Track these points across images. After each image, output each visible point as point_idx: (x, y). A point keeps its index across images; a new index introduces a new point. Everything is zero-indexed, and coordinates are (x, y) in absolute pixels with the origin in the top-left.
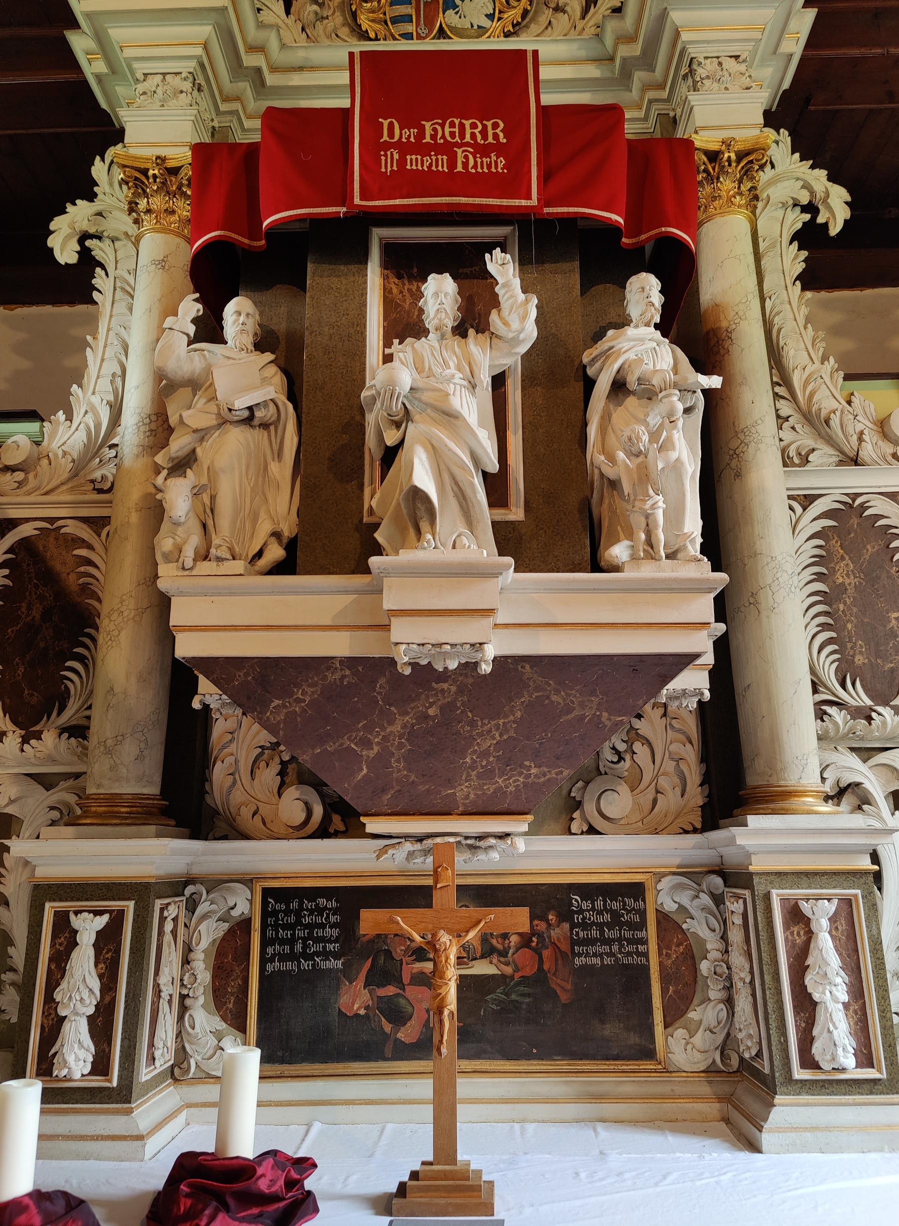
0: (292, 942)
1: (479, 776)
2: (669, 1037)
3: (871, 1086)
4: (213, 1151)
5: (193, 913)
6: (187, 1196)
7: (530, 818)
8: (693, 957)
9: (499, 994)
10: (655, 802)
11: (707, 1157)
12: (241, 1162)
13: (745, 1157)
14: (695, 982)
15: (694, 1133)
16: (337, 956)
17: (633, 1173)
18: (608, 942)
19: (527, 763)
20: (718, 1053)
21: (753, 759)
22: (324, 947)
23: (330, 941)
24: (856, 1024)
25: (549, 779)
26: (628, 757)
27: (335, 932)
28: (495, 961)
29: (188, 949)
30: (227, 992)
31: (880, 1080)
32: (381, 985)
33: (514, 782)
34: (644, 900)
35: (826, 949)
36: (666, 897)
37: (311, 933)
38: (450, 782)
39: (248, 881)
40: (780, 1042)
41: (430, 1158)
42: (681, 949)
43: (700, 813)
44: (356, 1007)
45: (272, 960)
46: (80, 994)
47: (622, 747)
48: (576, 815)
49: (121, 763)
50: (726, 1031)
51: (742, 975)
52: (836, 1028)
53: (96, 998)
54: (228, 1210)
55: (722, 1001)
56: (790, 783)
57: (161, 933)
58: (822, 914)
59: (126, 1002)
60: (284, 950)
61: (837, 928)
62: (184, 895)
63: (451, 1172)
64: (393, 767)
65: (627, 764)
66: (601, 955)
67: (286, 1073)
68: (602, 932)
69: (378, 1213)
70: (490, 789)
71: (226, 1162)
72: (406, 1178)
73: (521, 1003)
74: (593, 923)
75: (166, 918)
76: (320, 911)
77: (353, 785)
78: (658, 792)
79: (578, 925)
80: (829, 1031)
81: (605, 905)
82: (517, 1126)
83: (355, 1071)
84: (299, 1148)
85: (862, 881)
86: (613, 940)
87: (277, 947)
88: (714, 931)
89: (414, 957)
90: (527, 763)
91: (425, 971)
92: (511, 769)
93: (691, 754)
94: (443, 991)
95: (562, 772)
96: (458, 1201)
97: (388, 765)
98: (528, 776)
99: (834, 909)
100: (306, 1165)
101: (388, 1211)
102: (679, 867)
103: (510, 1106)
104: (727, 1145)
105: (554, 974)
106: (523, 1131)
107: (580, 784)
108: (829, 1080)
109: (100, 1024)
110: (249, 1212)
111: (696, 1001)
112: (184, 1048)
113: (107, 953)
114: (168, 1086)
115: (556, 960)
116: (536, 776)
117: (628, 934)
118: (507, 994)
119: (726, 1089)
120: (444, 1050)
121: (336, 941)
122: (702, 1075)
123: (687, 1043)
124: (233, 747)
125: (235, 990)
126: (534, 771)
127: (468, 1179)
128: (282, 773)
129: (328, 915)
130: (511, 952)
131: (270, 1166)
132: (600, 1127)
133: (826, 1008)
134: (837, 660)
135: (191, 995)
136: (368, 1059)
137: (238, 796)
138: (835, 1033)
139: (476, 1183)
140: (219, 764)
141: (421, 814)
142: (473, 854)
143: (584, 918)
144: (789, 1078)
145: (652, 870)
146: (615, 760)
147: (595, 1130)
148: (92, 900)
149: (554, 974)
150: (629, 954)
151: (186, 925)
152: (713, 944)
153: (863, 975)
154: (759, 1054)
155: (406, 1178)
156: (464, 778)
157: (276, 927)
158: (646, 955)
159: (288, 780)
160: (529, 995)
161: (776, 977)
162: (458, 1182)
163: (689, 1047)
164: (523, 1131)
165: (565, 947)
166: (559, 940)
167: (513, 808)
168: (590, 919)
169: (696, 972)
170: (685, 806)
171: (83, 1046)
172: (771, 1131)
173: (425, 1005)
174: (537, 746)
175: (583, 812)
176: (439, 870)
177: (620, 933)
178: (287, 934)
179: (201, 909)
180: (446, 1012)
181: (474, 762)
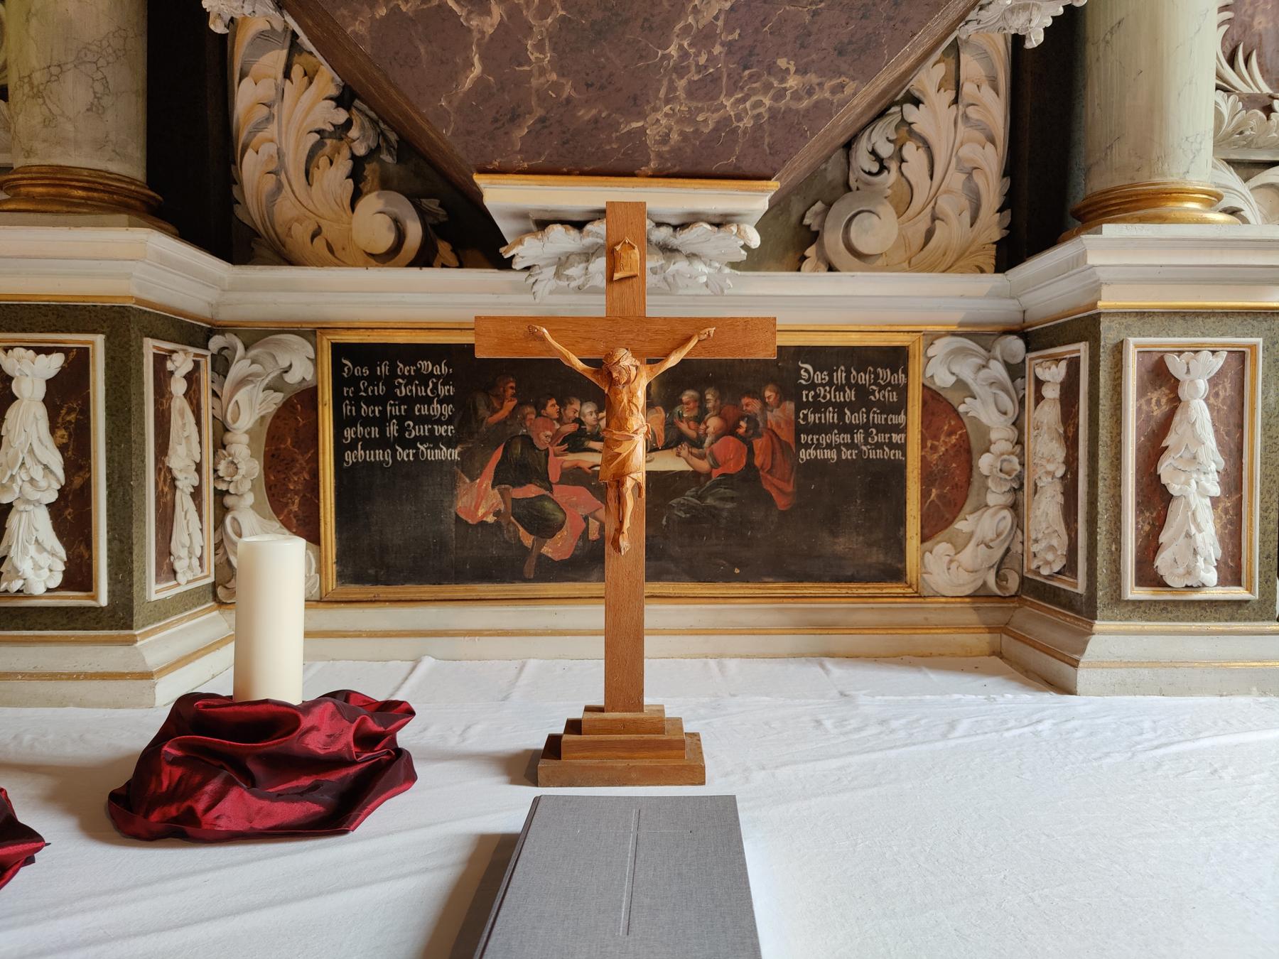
0: (382, 422)
1: (691, 93)
2: (927, 554)
3: (1234, 609)
4: (231, 694)
5: (225, 377)
6: (175, 762)
7: (774, 185)
8: (969, 451)
9: (689, 497)
10: (929, 234)
11: (1000, 699)
12: (273, 708)
13: (1050, 700)
14: (969, 483)
15: (962, 669)
16: (450, 443)
17: (903, 721)
18: (849, 429)
19: (782, 63)
20: (993, 572)
21: (1111, 147)
22: (431, 431)
23: (439, 422)
24: (1224, 527)
25: (817, 103)
26: (894, 166)
27: (447, 410)
28: (684, 452)
29: (222, 430)
30: (288, 490)
31: (1247, 601)
32: (518, 483)
33: (755, 106)
34: (906, 372)
35: (1199, 416)
36: (939, 368)
37: (410, 411)
38: (636, 105)
39: (310, 332)
40: (1110, 551)
41: (599, 701)
42: (954, 439)
43: (994, 253)
44: (481, 512)
45: (352, 447)
46: (28, 470)
47: (886, 150)
48: (810, 252)
49: (63, 114)
50: (1006, 545)
51: (1050, 467)
52: (1200, 531)
53: (58, 480)
54: (251, 781)
55: (1004, 507)
56: (1170, 179)
57: (162, 391)
58: (1199, 375)
59: (109, 486)
60: (370, 433)
61: (1217, 395)
62: (206, 348)
63: (634, 721)
64: (529, 62)
65: (891, 177)
66: (838, 447)
67: (383, 597)
68: (842, 416)
69: (514, 781)
70: (708, 120)
71: (245, 709)
72: (559, 729)
73: (723, 509)
74: (829, 403)
75: (172, 373)
76: (424, 379)
77: (456, 104)
78: (934, 218)
79: (807, 405)
80: (1188, 535)
81: (848, 378)
82: (712, 662)
83: (482, 595)
84: (398, 688)
85: (1265, 325)
86: (858, 427)
87: (360, 429)
88: (1005, 413)
89: (566, 446)
90: (782, 63)
91: (582, 465)
92: (751, 76)
93: (991, 160)
94: (623, 449)
95: (842, 87)
96: (647, 763)
97: (521, 59)
98: (780, 95)
99: (1221, 363)
100: (398, 712)
101: (532, 778)
102: (960, 325)
103: (702, 638)
104: (1014, 684)
105: (770, 472)
106: (722, 669)
107: (819, 206)
108: (1174, 601)
109: (70, 516)
110: (294, 783)
111: (967, 508)
112: (229, 562)
113: (68, 413)
114: (210, 610)
115: (773, 453)
116: (796, 96)
117: (879, 419)
118: (700, 498)
119: (998, 617)
120: (624, 543)
121: (449, 422)
122: (967, 600)
123: (951, 561)
124: (272, 130)
125: (300, 487)
126: (792, 82)
127: (661, 731)
128: (356, 174)
129: (435, 385)
130: (708, 440)
131: (327, 714)
132: (828, 663)
133: (1188, 505)
134: (1229, 21)
135: (232, 491)
136: (501, 580)
137: (286, 209)
138: (1199, 537)
139: (677, 738)
140: (250, 154)
141: (583, 173)
142: (668, 260)
143: (816, 396)
144: (1117, 598)
145: (922, 328)
146: (875, 168)
147: (822, 666)
148: (32, 331)
149: (770, 472)
150: (878, 446)
151: (215, 394)
152: (1000, 433)
153: (1246, 460)
154: (1070, 568)
155: (559, 729)
156: (662, 94)
157: (356, 401)
158: (902, 447)
159: (365, 187)
160: (732, 499)
161: (1116, 462)
162: (646, 736)
163: (954, 566)
164: (722, 669)
165: (786, 435)
166: (779, 425)
167: (746, 165)
168: (824, 397)
169: (971, 470)
170: (974, 241)
171: (45, 550)
172: (1091, 666)
173: (582, 511)
174: (808, 18)
175: (821, 246)
176: (618, 248)
177: (868, 418)
178: (373, 412)
179: (239, 368)
180: (629, 483)
181: (684, 55)
